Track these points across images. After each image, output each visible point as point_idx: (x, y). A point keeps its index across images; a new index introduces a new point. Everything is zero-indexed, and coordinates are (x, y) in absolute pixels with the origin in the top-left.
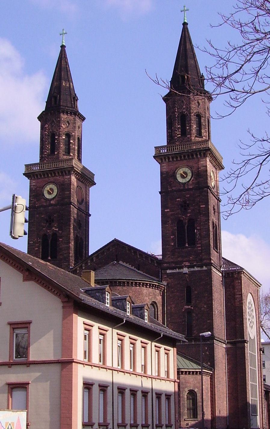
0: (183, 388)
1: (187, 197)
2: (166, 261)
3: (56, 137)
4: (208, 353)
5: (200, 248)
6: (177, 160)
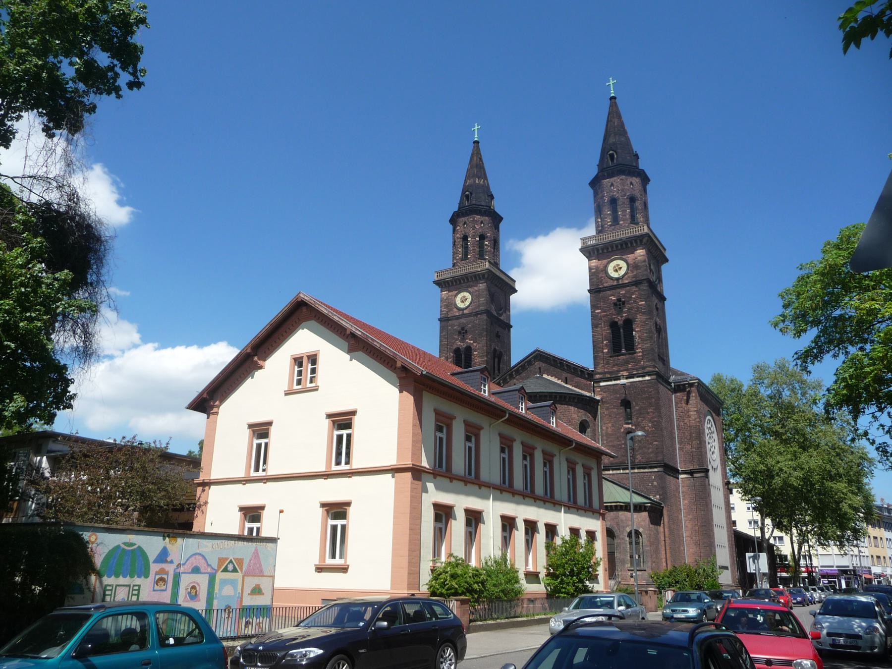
0: (624, 527)
1: (622, 294)
2: (599, 371)
3: (469, 239)
4: (655, 483)
5: (641, 354)
6: (608, 252)
